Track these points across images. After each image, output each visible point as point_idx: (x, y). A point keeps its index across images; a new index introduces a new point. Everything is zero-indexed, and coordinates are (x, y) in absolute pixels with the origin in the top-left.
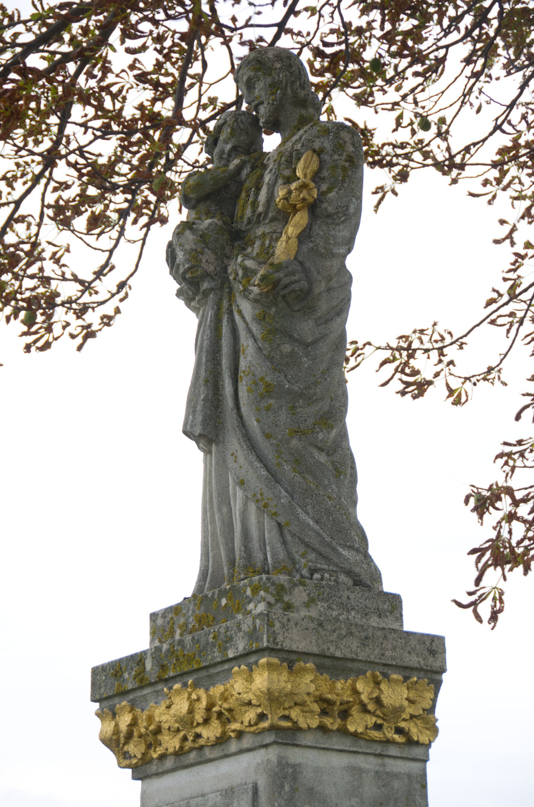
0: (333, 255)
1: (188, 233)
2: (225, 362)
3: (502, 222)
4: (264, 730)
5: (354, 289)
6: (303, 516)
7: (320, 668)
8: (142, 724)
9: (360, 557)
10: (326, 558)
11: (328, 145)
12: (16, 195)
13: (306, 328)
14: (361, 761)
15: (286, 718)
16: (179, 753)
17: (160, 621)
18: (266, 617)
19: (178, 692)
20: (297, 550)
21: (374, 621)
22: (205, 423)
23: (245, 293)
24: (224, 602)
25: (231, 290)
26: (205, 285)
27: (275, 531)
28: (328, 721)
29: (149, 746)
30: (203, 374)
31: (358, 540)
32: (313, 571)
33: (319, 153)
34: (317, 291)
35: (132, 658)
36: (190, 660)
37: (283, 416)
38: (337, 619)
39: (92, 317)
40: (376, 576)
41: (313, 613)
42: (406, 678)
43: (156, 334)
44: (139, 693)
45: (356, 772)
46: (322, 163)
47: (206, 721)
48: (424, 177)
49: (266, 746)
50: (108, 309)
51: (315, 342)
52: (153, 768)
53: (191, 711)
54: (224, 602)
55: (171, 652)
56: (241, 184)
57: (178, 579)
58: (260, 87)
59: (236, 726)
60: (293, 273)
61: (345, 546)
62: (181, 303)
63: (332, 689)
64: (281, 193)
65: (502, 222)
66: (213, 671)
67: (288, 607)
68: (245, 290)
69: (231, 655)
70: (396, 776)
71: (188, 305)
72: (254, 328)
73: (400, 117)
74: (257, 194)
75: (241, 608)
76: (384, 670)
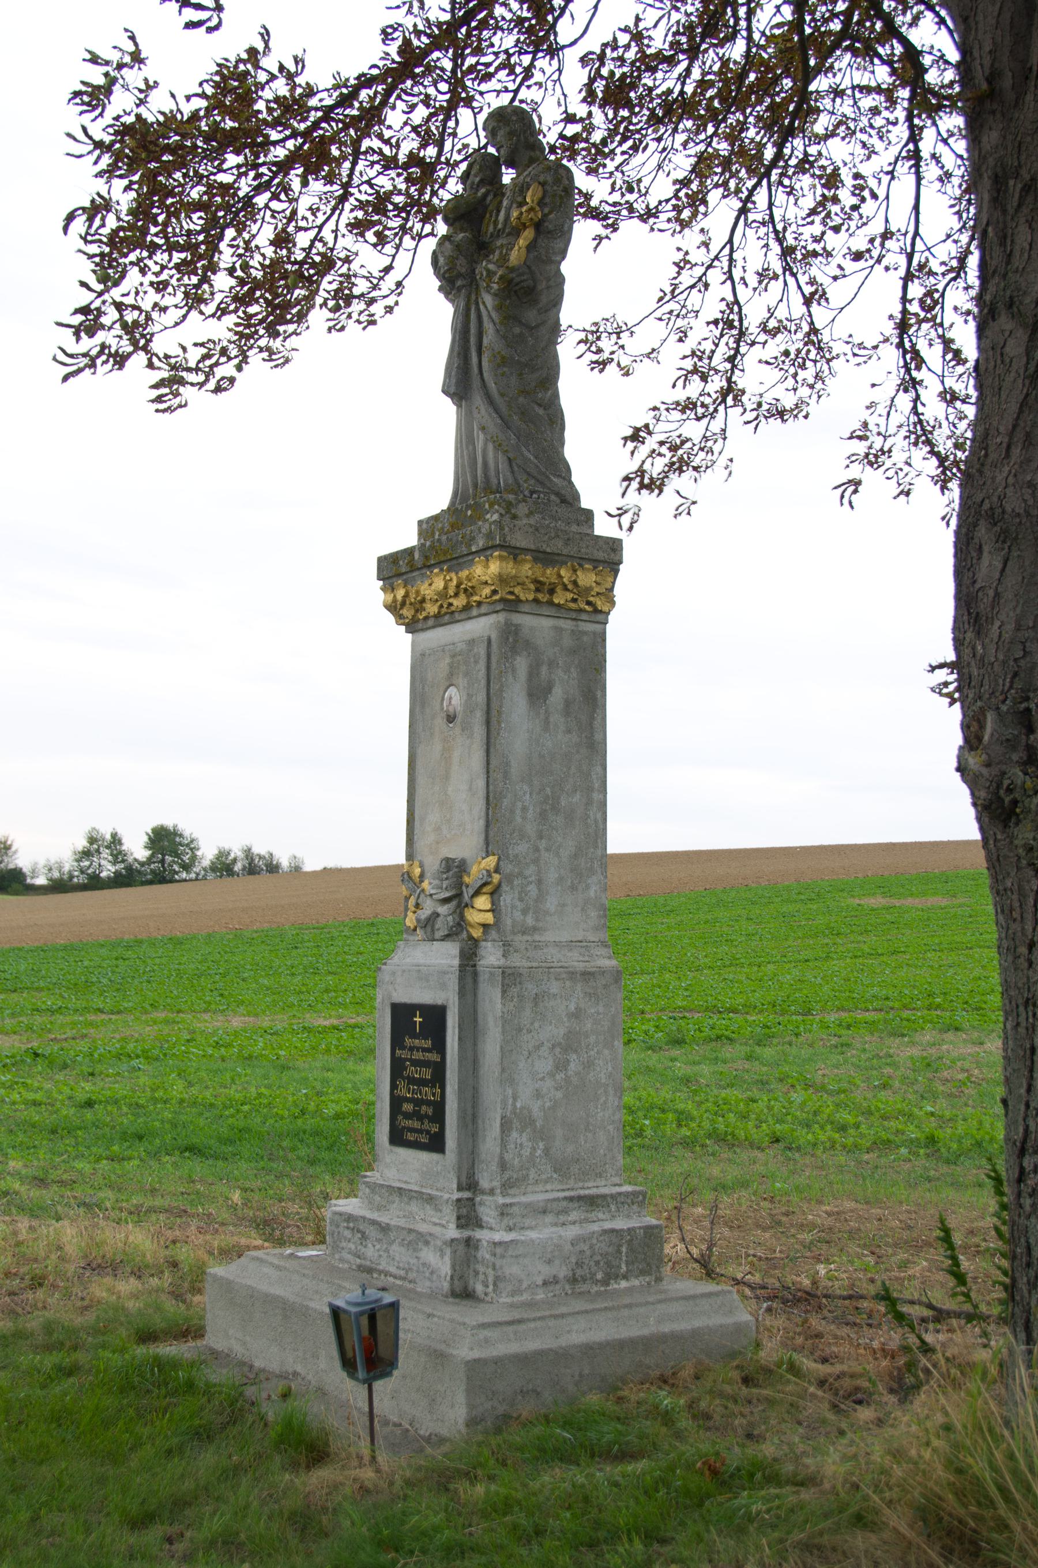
0: (552, 262)
1: (447, 244)
2: (473, 340)
3: (679, 249)
4: (496, 601)
5: (566, 287)
6: (526, 453)
7: (536, 560)
8: (412, 596)
9: (565, 483)
10: (542, 483)
11: (549, 179)
12: (319, 222)
13: (531, 316)
14: (561, 623)
15: (512, 593)
16: (437, 616)
17: (424, 526)
18: (499, 524)
19: (437, 575)
20: (522, 477)
21: (574, 528)
22: (457, 384)
23: (488, 288)
24: (469, 513)
25: (477, 286)
26: (459, 283)
27: (506, 464)
28: (540, 596)
29: (417, 611)
30: (456, 349)
31: (564, 471)
32: (532, 492)
33: (543, 184)
34: (539, 288)
35: (405, 551)
36: (445, 553)
37: (514, 381)
38: (548, 526)
39: (377, 309)
40: (576, 497)
41: (532, 521)
42: (595, 568)
43: (423, 319)
44: (410, 575)
45: (559, 630)
46: (545, 192)
47: (456, 595)
48: (630, 227)
49: (497, 612)
50: (390, 301)
51: (537, 326)
52: (420, 625)
53: (446, 588)
54: (469, 513)
55: (432, 547)
56: (486, 207)
57: (438, 497)
58: (501, 133)
59: (476, 598)
60: (522, 274)
61: (555, 475)
62: (442, 296)
63: (544, 574)
64: (515, 214)
65: (679, 249)
66: (461, 560)
67: (514, 517)
68: (488, 286)
69: (474, 549)
70: (585, 633)
71: (447, 298)
72: (494, 315)
73: (614, 183)
74: (497, 215)
75: (481, 517)
76: (580, 561)
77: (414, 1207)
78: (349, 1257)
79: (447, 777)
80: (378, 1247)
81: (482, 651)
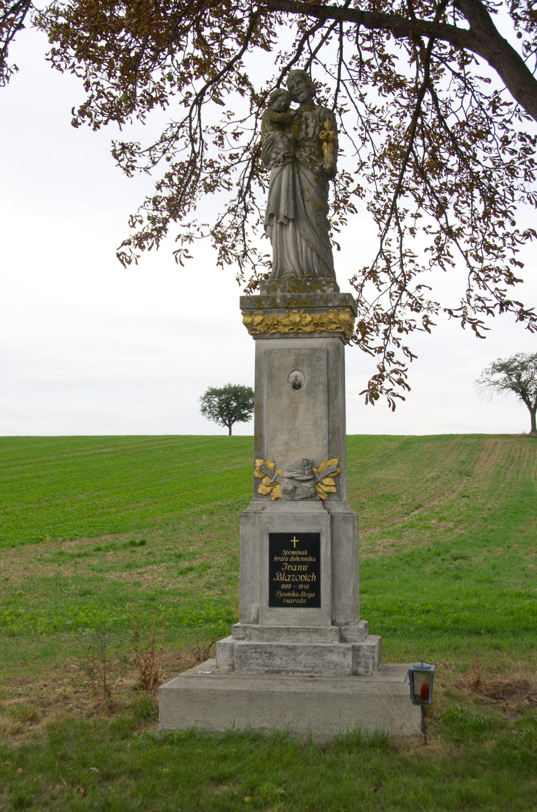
36: (305, 303)
77: (301, 636)
78: (259, 668)
79: (295, 417)
80: (285, 658)
81: (324, 356)
